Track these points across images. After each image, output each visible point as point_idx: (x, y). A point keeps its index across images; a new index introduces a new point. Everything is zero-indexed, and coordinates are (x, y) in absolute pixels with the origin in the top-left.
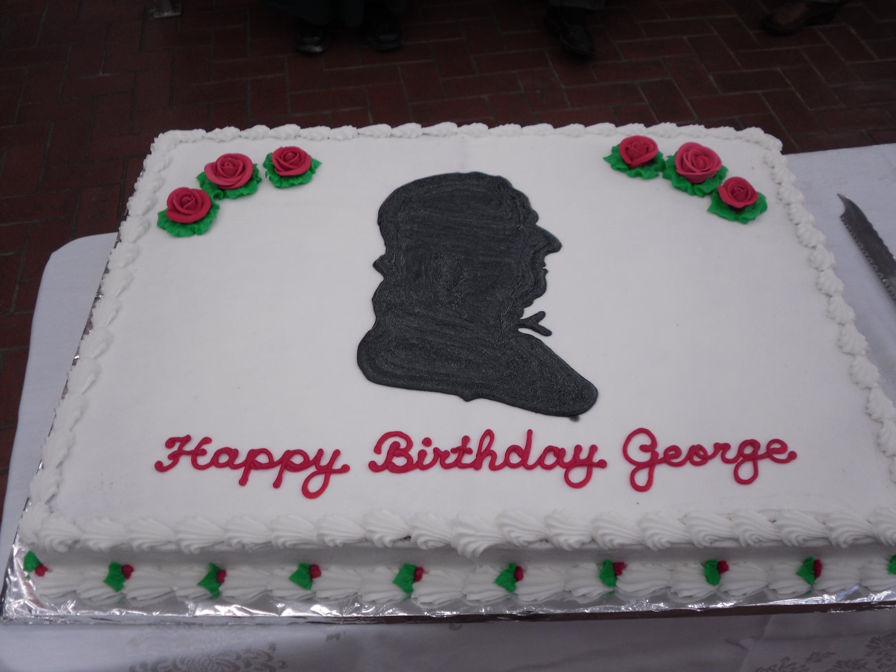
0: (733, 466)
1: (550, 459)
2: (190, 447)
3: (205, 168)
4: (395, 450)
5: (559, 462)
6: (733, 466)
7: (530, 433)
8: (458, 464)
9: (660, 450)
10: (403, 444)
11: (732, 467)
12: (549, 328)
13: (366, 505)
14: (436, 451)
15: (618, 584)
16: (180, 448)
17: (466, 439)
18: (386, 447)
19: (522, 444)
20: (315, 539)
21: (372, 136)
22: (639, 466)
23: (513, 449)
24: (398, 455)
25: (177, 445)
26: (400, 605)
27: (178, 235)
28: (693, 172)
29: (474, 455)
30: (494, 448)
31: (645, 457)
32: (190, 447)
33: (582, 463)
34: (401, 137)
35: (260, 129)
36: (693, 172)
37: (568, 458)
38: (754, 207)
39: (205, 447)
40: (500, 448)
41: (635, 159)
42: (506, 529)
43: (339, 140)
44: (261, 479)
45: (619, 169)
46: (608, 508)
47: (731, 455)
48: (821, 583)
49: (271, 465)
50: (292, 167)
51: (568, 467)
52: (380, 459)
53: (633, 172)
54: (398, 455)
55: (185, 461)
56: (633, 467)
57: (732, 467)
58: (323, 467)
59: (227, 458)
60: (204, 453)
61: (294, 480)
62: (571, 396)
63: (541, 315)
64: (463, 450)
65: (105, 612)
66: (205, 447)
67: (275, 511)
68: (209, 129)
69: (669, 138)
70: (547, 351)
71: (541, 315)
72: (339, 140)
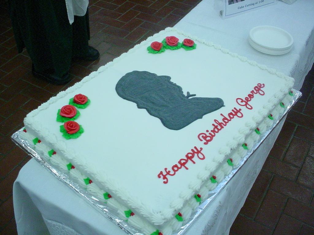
0: (258, 93)
1: (231, 116)
2: (164, 173)
3: (166, 38)
4: (205, 138)
5: (233, 115)
6: (258, 93)
7: (221, 115)
8: (219, 130)
9: (244, 100)
10: (204, 135)
11: (258, 93)
12: (194, 94)
13: (215, 152)
14: (212, 131)
15: (260, 132)
16: (163, 175)
17: (213, 125)
18: (202, 139)
19: (223, 117)
20: (218, 164)
21: (87, 81)
22: (246, 105)
23: (223, 120)
24: (207, 138)
25: (161, 175)
26: (233, 169)
27: (78, 137)
28: (174, 43)
29: (218, 127)
30: (220, 122)
31: (244, 103)
32: (164, 173)
33: (235, 113)
34: (94, 77)
35: (61, 93)
36: (174, 43)
37: (234, 113)
38: (191, 47)
39: (167, 171)
40: (221, 121)
41: (156, 48)
42: (244, 132)
43: (80, 87)
44: (189, 164)
45: (59, 122)
46: (251, 117)
47: (255, 92)
48: (286, 106)
49: (187, 161)
50: (81, 100)
51: (236, 115)
52: (204, 141)
53: (160, 51)
54: (207, 138)
55: (168, 176)
56: (245, 106)
57: (258, 93)
58: (197, 151)
59: (176, 168)
60: (169, 172)
61: (195, 159)
62: (217, 104)
63: (188, 93)
64: (216, 127)
65: (192, 219)
66: (167, 171)
67: (198, 170)
68: (36, 108)
69: (160, 37)
70: (197, 99)
71: (188, 93)
72: (80, 87)
